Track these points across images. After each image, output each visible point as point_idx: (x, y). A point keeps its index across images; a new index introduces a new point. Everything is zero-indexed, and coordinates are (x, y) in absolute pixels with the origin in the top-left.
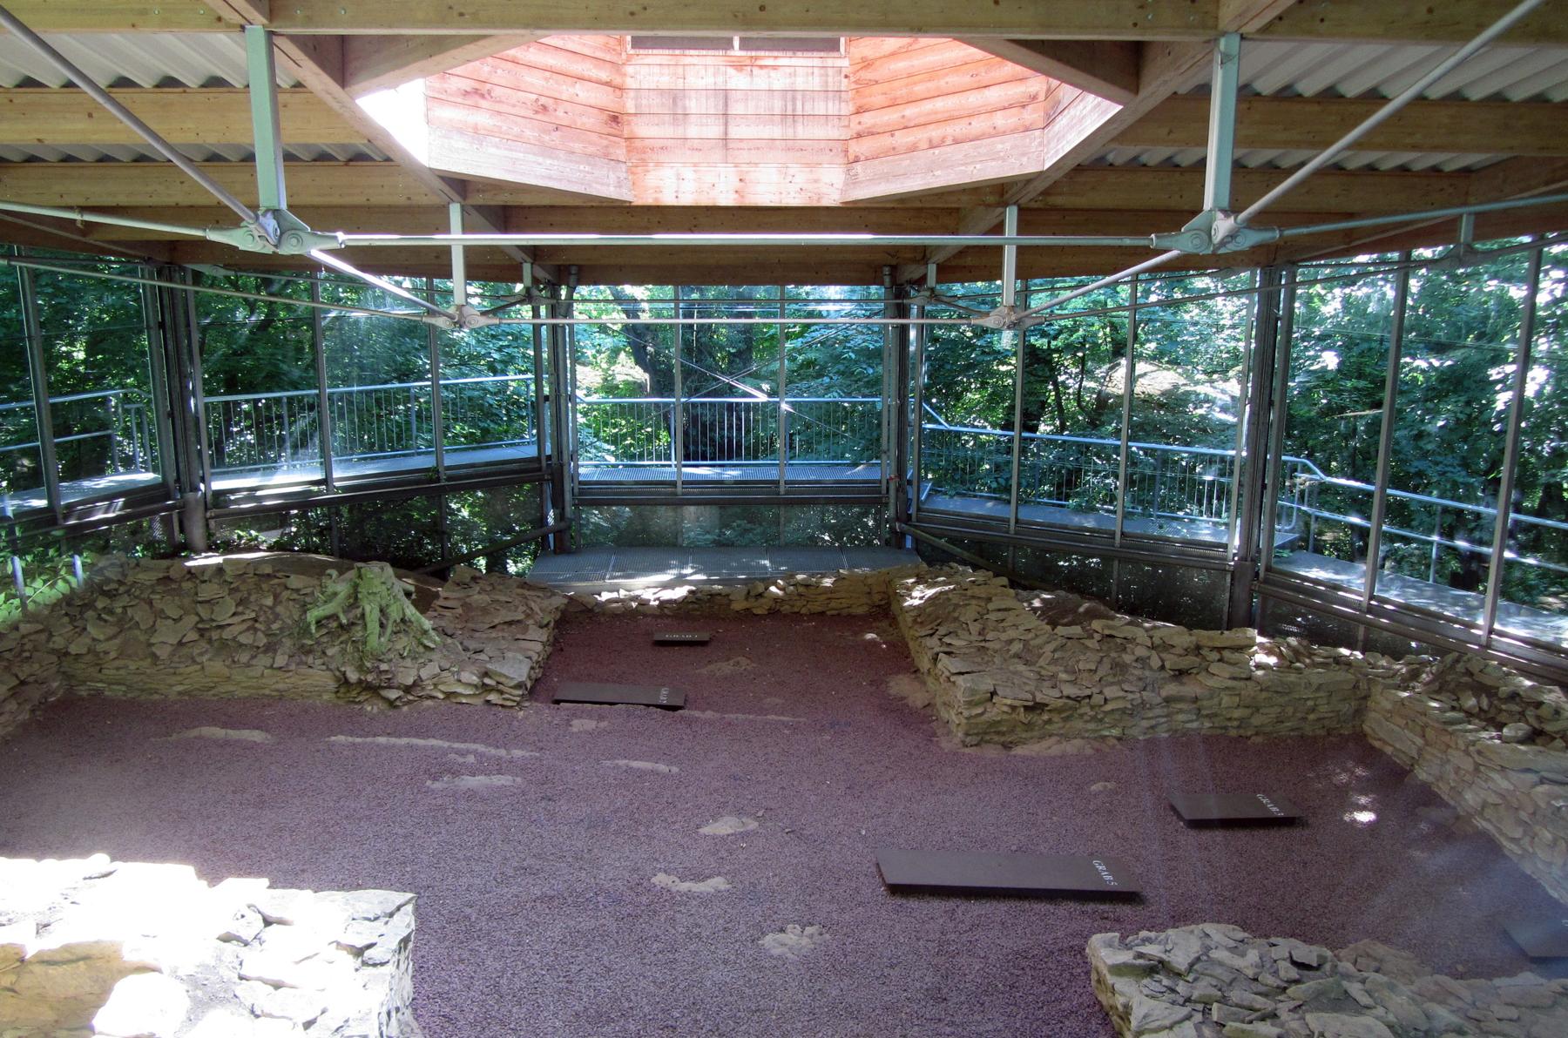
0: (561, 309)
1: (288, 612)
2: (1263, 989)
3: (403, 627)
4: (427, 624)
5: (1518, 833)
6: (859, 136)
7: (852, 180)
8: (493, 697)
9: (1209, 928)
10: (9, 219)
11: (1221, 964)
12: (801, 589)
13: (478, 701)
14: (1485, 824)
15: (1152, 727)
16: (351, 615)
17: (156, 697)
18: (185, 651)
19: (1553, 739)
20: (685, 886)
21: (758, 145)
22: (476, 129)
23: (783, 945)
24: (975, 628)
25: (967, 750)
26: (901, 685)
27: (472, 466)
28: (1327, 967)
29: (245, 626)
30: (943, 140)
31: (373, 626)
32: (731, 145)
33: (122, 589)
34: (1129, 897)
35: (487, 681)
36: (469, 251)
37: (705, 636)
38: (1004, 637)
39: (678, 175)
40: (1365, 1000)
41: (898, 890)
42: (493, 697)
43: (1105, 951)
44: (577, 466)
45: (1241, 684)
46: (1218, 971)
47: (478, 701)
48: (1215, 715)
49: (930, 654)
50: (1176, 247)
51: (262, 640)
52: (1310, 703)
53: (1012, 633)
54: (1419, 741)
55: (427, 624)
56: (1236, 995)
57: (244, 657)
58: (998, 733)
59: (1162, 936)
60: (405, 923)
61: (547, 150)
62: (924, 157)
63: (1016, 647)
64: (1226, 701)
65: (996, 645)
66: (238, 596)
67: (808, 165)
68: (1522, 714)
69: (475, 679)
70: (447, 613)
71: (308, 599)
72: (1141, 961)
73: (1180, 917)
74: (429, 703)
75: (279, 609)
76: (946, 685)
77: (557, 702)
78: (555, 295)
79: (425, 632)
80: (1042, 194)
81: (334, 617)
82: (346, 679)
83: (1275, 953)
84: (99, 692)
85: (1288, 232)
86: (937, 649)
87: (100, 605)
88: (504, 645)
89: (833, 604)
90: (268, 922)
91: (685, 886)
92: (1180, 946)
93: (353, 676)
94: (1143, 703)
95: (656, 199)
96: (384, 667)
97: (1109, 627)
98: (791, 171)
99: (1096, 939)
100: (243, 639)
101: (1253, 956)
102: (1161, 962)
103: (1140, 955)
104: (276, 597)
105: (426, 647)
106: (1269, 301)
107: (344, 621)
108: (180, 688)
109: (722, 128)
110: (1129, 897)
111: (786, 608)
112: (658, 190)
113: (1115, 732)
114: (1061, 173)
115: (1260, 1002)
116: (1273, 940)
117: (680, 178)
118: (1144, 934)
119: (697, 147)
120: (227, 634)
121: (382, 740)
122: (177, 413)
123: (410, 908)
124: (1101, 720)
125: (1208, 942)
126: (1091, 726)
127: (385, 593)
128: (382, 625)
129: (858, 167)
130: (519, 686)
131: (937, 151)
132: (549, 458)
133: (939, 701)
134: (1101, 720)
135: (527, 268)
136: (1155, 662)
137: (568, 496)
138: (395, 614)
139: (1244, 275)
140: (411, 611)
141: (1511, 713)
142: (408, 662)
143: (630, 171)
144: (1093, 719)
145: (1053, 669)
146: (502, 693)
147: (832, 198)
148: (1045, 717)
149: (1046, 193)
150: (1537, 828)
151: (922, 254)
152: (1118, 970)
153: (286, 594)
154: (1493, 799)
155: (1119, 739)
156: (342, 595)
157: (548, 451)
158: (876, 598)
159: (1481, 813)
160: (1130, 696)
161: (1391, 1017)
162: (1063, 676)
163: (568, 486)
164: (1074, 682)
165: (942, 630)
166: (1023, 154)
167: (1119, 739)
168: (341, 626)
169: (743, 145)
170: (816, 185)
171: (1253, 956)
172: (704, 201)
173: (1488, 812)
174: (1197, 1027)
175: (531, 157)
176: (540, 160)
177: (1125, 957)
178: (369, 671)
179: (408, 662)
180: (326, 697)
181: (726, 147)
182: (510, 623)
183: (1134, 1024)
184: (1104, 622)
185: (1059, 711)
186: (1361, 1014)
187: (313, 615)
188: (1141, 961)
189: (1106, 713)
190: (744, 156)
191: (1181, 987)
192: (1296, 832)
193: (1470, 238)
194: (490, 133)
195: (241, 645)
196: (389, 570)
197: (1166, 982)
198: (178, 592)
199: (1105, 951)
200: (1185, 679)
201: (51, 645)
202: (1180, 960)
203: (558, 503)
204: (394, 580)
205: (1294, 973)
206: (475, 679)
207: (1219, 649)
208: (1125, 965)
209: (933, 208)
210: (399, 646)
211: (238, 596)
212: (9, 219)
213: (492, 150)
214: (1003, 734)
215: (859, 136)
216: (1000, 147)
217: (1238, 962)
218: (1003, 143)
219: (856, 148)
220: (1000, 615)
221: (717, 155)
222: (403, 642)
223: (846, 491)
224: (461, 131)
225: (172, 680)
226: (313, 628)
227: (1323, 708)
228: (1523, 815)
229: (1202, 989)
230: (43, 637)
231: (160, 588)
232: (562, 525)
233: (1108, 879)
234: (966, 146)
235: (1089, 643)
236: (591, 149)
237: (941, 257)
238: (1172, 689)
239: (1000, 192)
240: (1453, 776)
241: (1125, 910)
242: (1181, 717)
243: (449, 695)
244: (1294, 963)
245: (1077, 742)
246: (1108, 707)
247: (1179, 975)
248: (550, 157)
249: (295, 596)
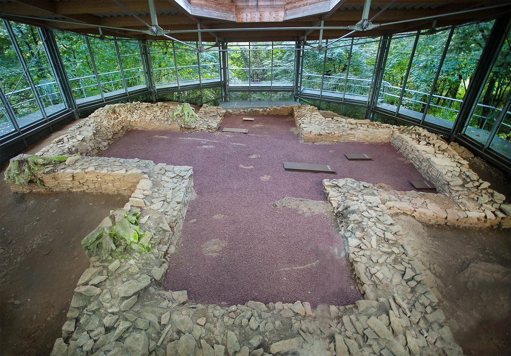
0: (225, 47)
1: (170, 113)
2: (356, 191)
3: (192, 116)
4: (197, 116)
5: (418, 164)
6: (288, 4)
7: (286, 15)
8: (210, 130)
9: (347, 179)
10: (108, 30)
11: (349, 186)
12: (274, 110)
13: (207, 131)
14: (412, 162)
15: (344, 140)
16: (182, 114)
17: (147, 130)
18: (152, 121)
19: (431, 144)
20: (245, 167)
21: (265, 7)
22: (201, 5)
23: (263, 179)
24: (309, 118)
25: (305, 143)
26: (293, 129)
27: (207, 83)
28: (370, 188)
29: (163, 116)
30: (307, 4)
31: (186, 116)
32: (258, 7)
33: (139, 109)
34: (333, 173)
35: (209, 127)
36: (202, 33)
37: (253, 119)
38: (315, 120)
39: (247, 15)
40: (377, 194)
41: (286, 169)
42: (210, 130)
43: (326, 182)
44: (229, 83)
45: (364, 131)
46: (348, 187)
47: (207, 131)
48: (358, 137)
49: (299, 123)
50: (356, 28)
51: (166, 119)
52: (379, 136)
53: (317, 119)
54: (401, 144)
55: (197, 116)
56: (350, 192)
57: (163, 122)
58: (311, 140)
59: (338, 180)
60: (191, 172)
61: (217, 10)
62: (302, 8)
63: (317, 122)
64: (361, 135)
65: (313, 122)
66: (161, 110)
67: (276, 11)
68: (425, 139)
69: (206, 127)
70: (201, 114)
71: (174, 111)
72: (332, 185)
73: (343, 177)
74: (198, 131)
75: (169, 113)
76: (302, 130)
77: (223, 132)
78: (223, 44)
79: (197, 117)
80: (329, 17)
81: (179, 114)
82: (182, 127)
83: (360, 184)
84: (137, 129)
85: (382, 25)
86: (300, 123)
87: (136, 112)
88: (212, 120)
89: (281, 113)
90: (166, 171)
91: (245, 167)
92: (341, 182)
93: (183, 126)
94: (343, 135)
95: (242, 21)
96: (189, 124)
97: (337, 119)
98: (272, 13)
99: (325, 180)
100: (162, 119)
101: (355, 184)
102: (337, 185)
103: (333, 183)
104: (168, 110)
105: (197, 120)
106: (384, 43)
107: (181, 115)
108: (152, 128)
109: (256, 3)
110: (333, 173)
111: (270, 114)
112: (242, 19)
113: (336, 140)
114: (333, 12)
115: (355, 193)
116: (360, 182)
117: (247, 15)
118: (334, 180)
119: (251, 8)
120: (159, 118)
121: (189, 138)
122: (148, 73)
123: (192, 169)
124: (333, 138)
125: (347, 182)
126: (331, 139)
127: (188, 109)
128: (188, 116)
129: (287, 12)
130: (215, 128)
131: (305, 7)
132: (223, 81)
133: (300, 133)
134: (333, 138)
135: (216, 38)
136: (346, 126)
137: (227, 90)
138: (191, 114)
139: (379, 38)
140: (194, 113)
141: (423, 139)
142: (193, 123)
143: (236, 14)
144: (332, 138)
145: (324, 127)
146: (212, 130)
147: (281, 20)
148: (322, 137)
149: (331, 17)
150: (423, 163)
151: (304, 32)
152: (328, 186)
153: (170, 110)
154: (415, 157)
155: (337, 142)
156: (180, 110)
157: (223, 80)
158: (290, 112)
159: (412, 159)
160: (340, 133)
161: (381, 197)
162: (326, 128)
163: (227, 88)
164: (328, 130)
165: (302, 119)
166: (325, 7)
167: (337, 142)
168: (180, 116)
169: (261, 7)
170: (277, 16)
171: (355, 184)
172: (252, 21)
173: (413, 159)
174: (342, 197)
175: (214, 12)
176: (216, 12)
177: (330, 184)
178: (186, 125)
179: (193, 123)
180: (178, 130)
181: (257, 7)
182: (214, 116)
183: (329, 196)
184: (336, 117)
185: (324, 136)
186: (375, 196)
187: (175, 114)
188: (332, 185)
189: (335, 136)
190: (261, 10)
191: (340, 190)
192: (371, 162)
193: (434, 27)
194: (205, 6)
195: (162, 120)
196: (189, 105)
197: (337, 189)
198: (150, 109)
199: (326, 182)
200: (352, 130)
201: (128, 120)
202: (340, 185)
203: (225, 91)
204: (190, 107)
205: (363, 188)
206: (206, 127)
207: (361, 124)
208: (329, 185)
209: (306, 22)
210: (192, 120)
211: (161, 110)
212: (108, 30)
213: (205, 10)
214: (313, 140)
215: (288, 4)
216: (320, 5)
217: (352, 186)
218: (320, 4)
219: (287, 7)
220: (315, 116)
221: (255, 10)
222: (192, 119)
223: (285, 88)
224: (198, 6)
225: (150, 126)
226: (175, 116)
227: (381, 137)
228: (420, 160)
229: (344, 190)
230: (126, 118)
231: (146, 109)
232: (226, 96)
233: (329, 169)
234: (312, 5)
235: (333, 122)
236: (227, 9)
237: (308, 34)
238: (349, 132)
239: (320, 17)
240: (407, 152)
241: (332, 176)
242: (350, 138)
243: (201, 130)
244: (363, 186)
245: (328, 142)
246: (335, 135)
247: (340, 187)
248: (218, 11)
249: (172, 110)
